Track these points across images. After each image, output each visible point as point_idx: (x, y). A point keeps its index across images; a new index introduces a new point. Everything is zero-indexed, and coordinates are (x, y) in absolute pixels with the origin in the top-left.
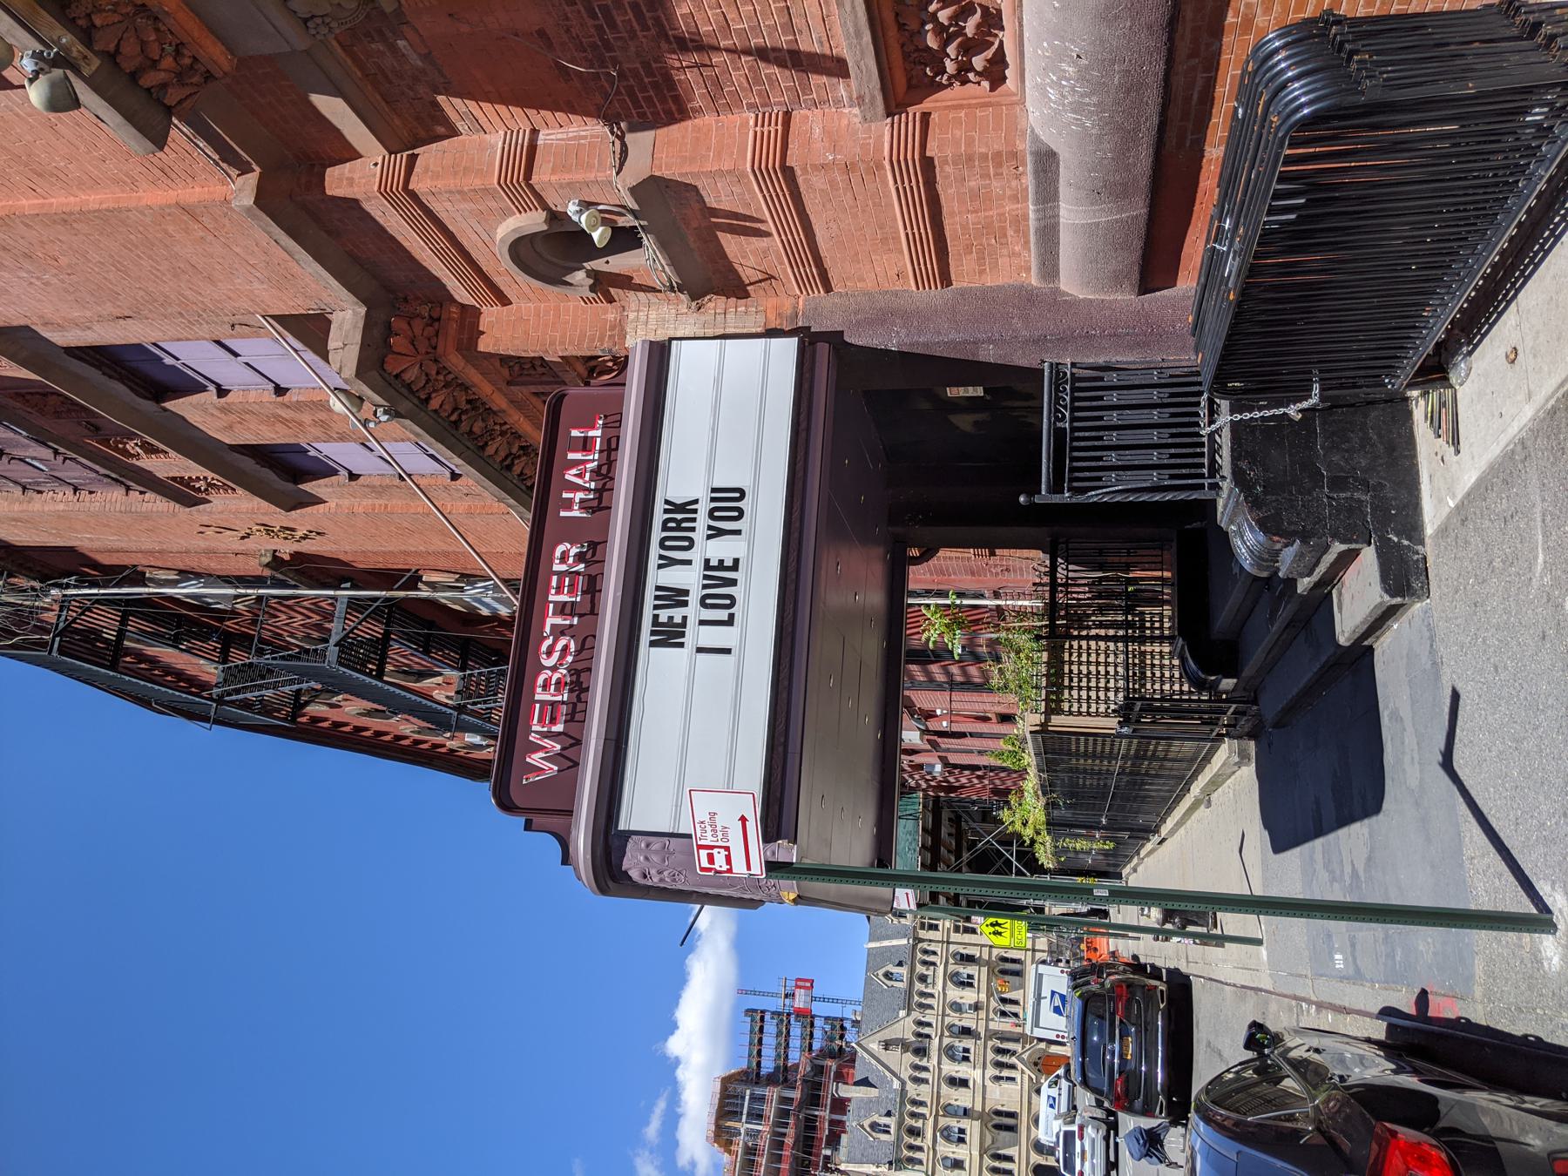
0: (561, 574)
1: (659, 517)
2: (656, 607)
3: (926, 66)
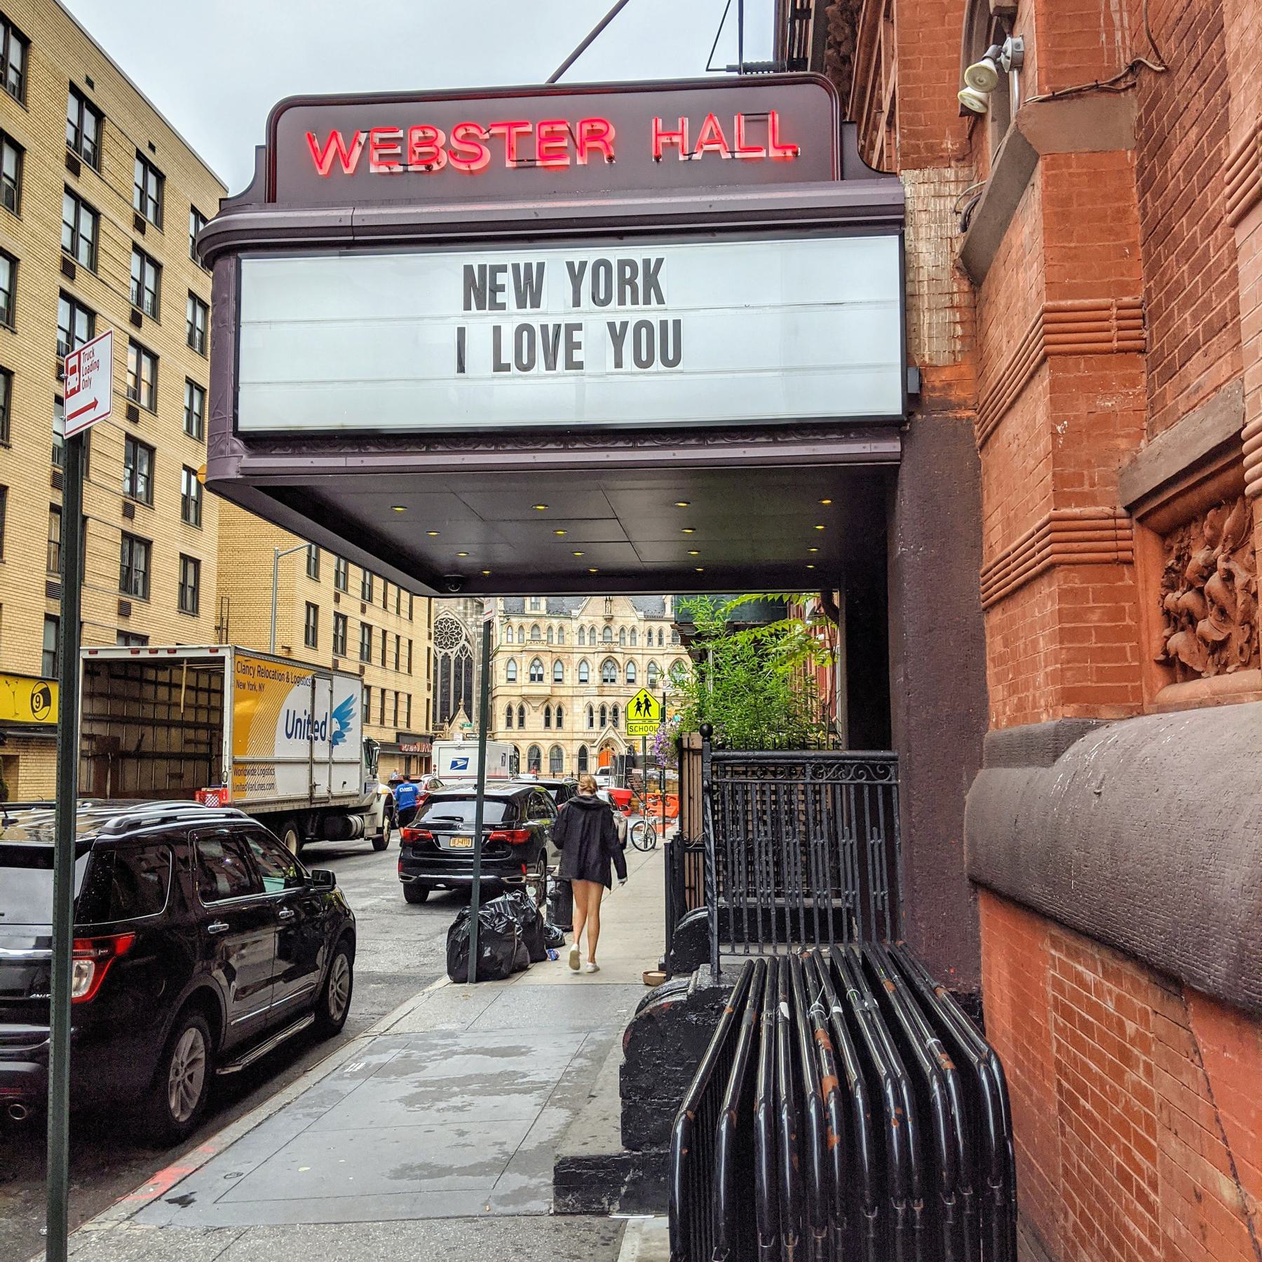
1: (639, 253)
2: (516, 267)
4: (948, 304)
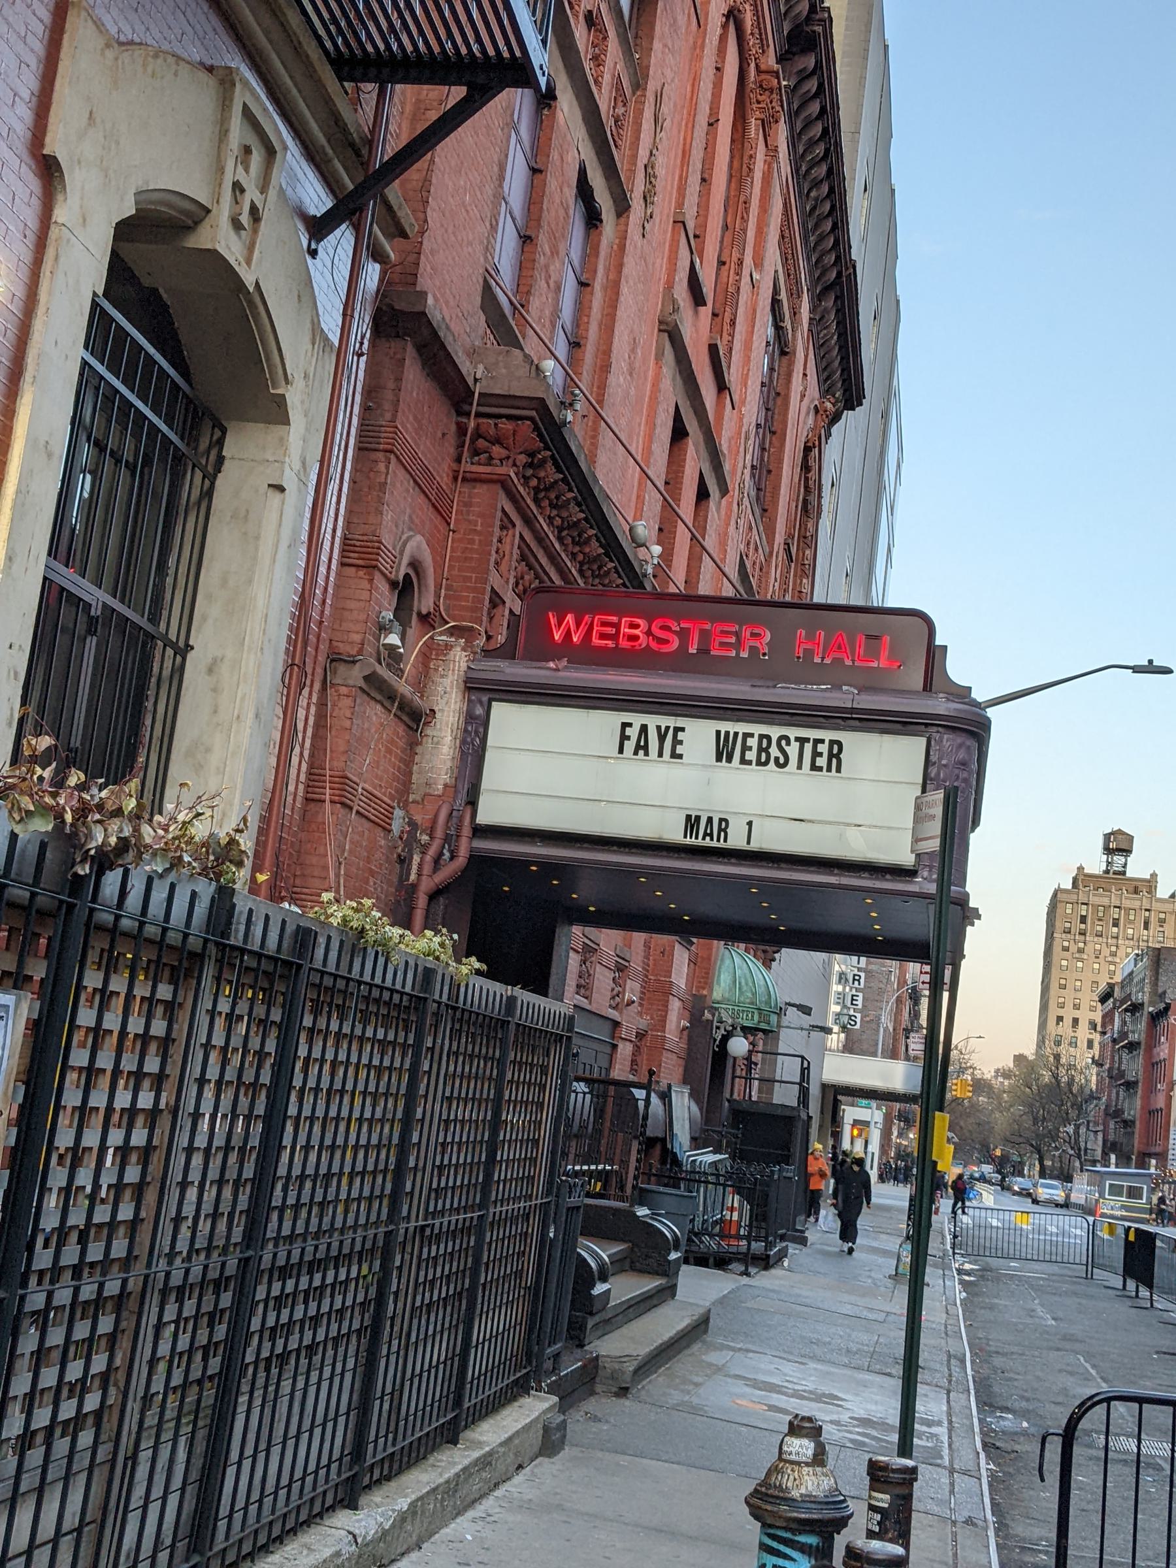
3: (669, 1262)
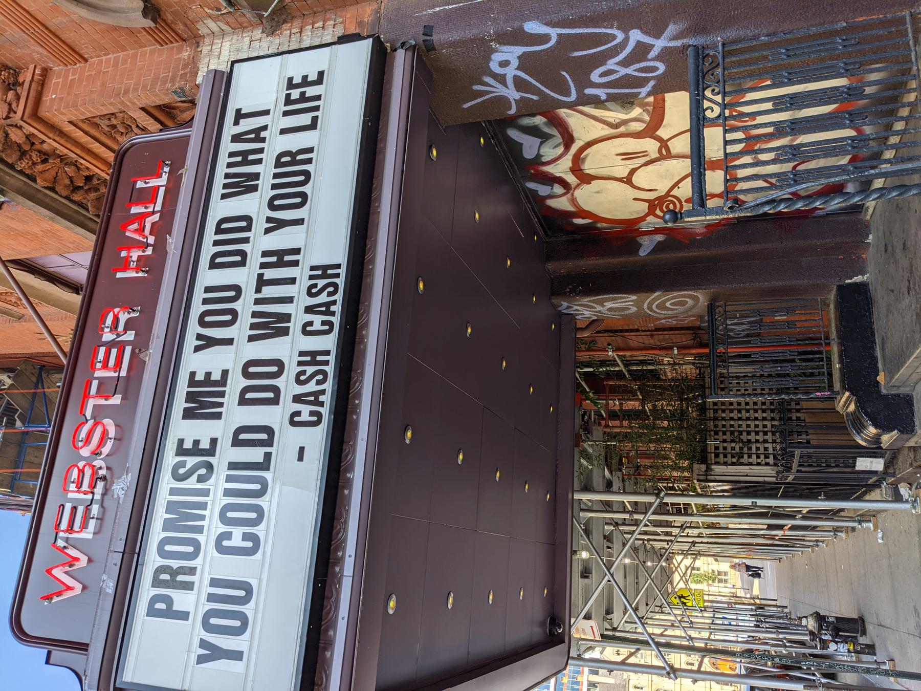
0: (110, 345)
4: (298, 35)
